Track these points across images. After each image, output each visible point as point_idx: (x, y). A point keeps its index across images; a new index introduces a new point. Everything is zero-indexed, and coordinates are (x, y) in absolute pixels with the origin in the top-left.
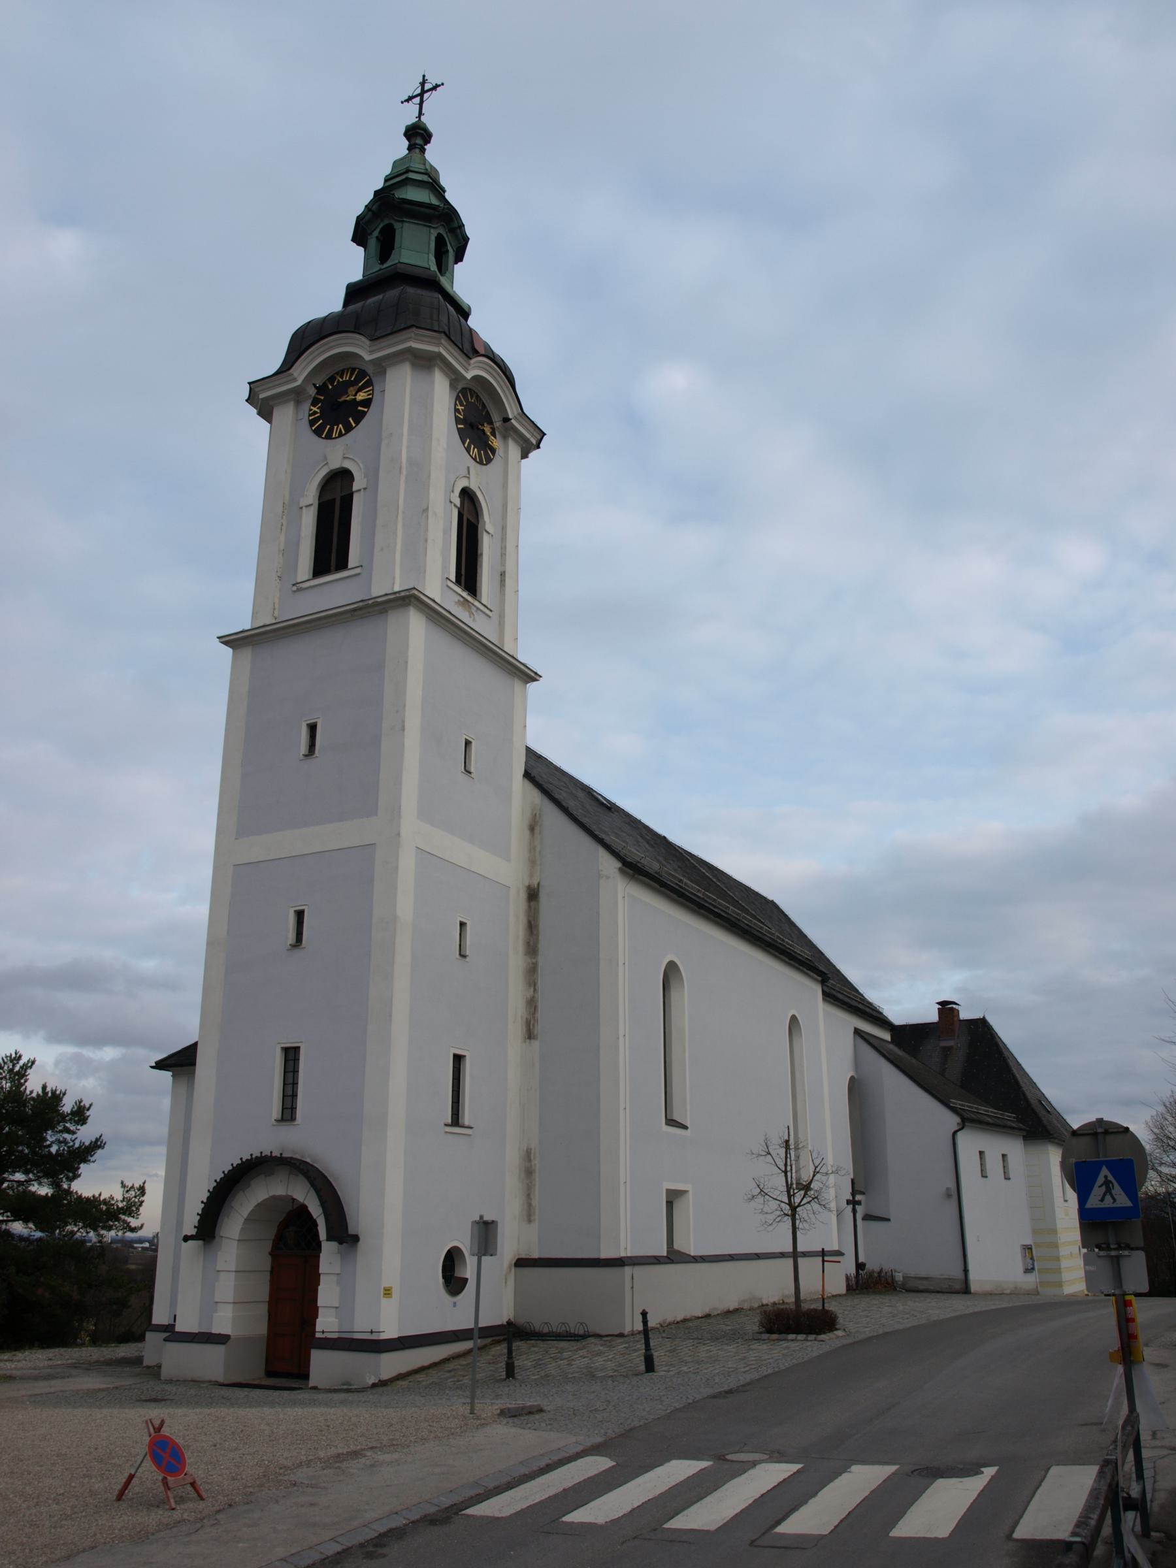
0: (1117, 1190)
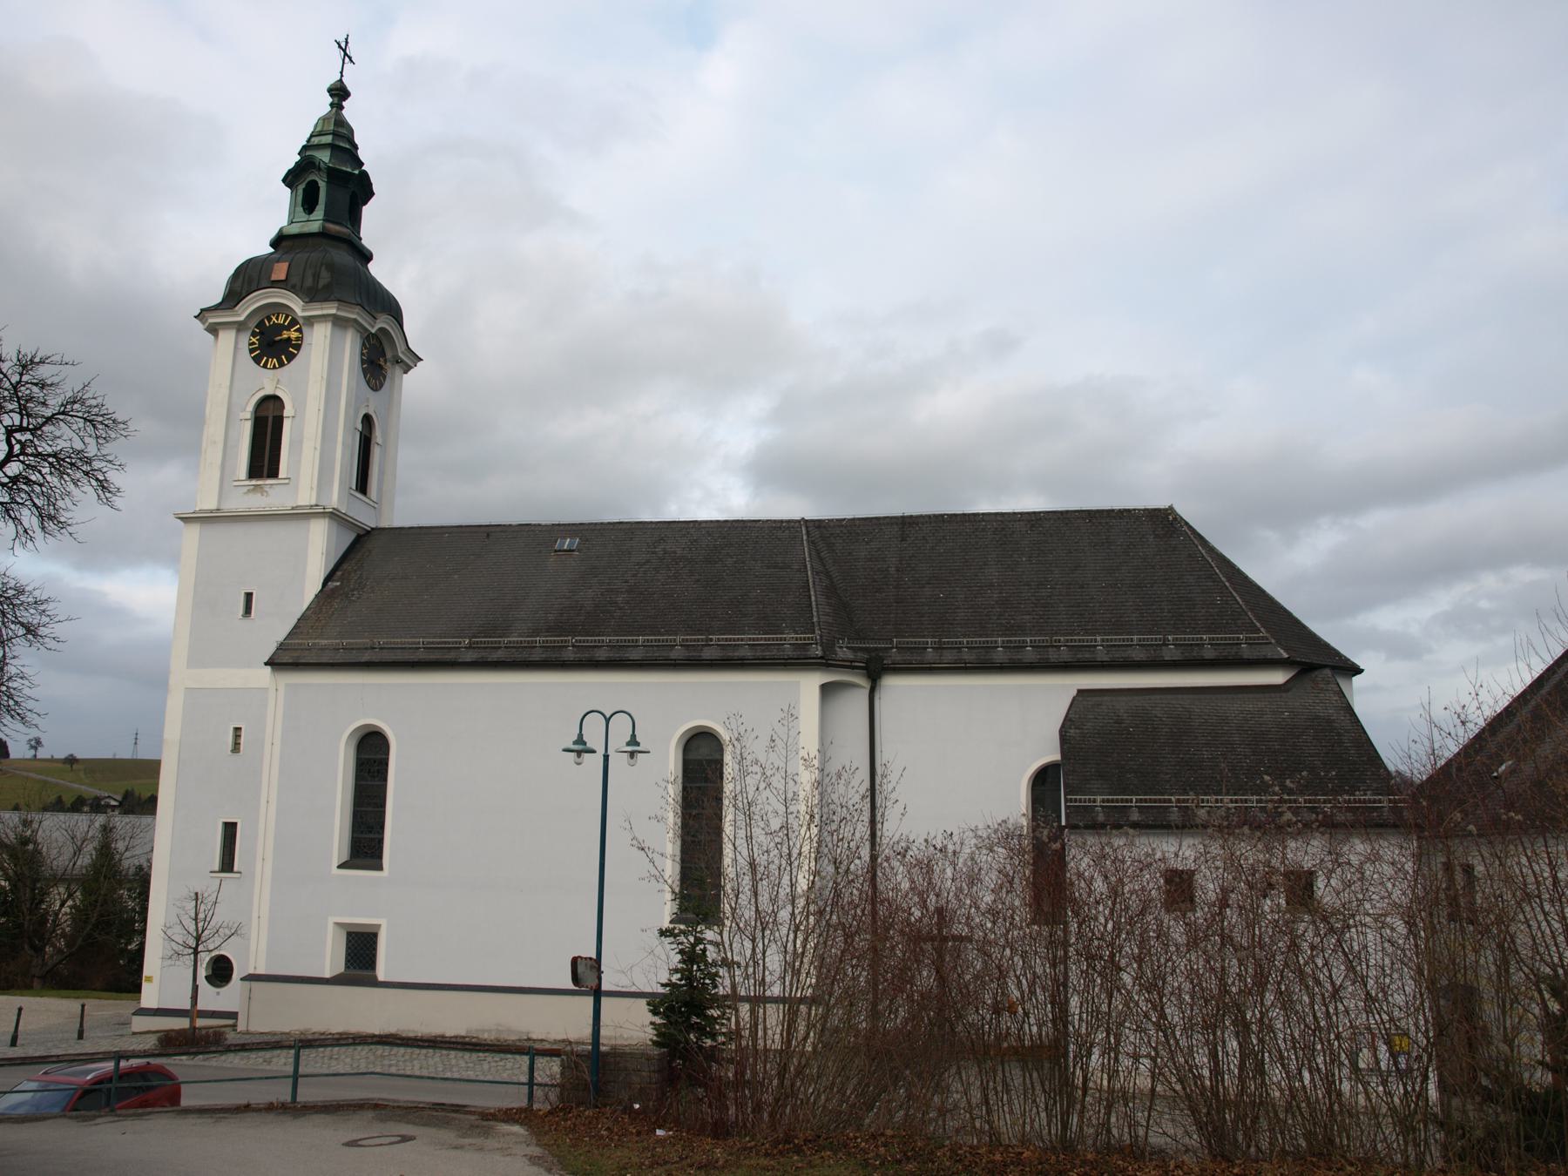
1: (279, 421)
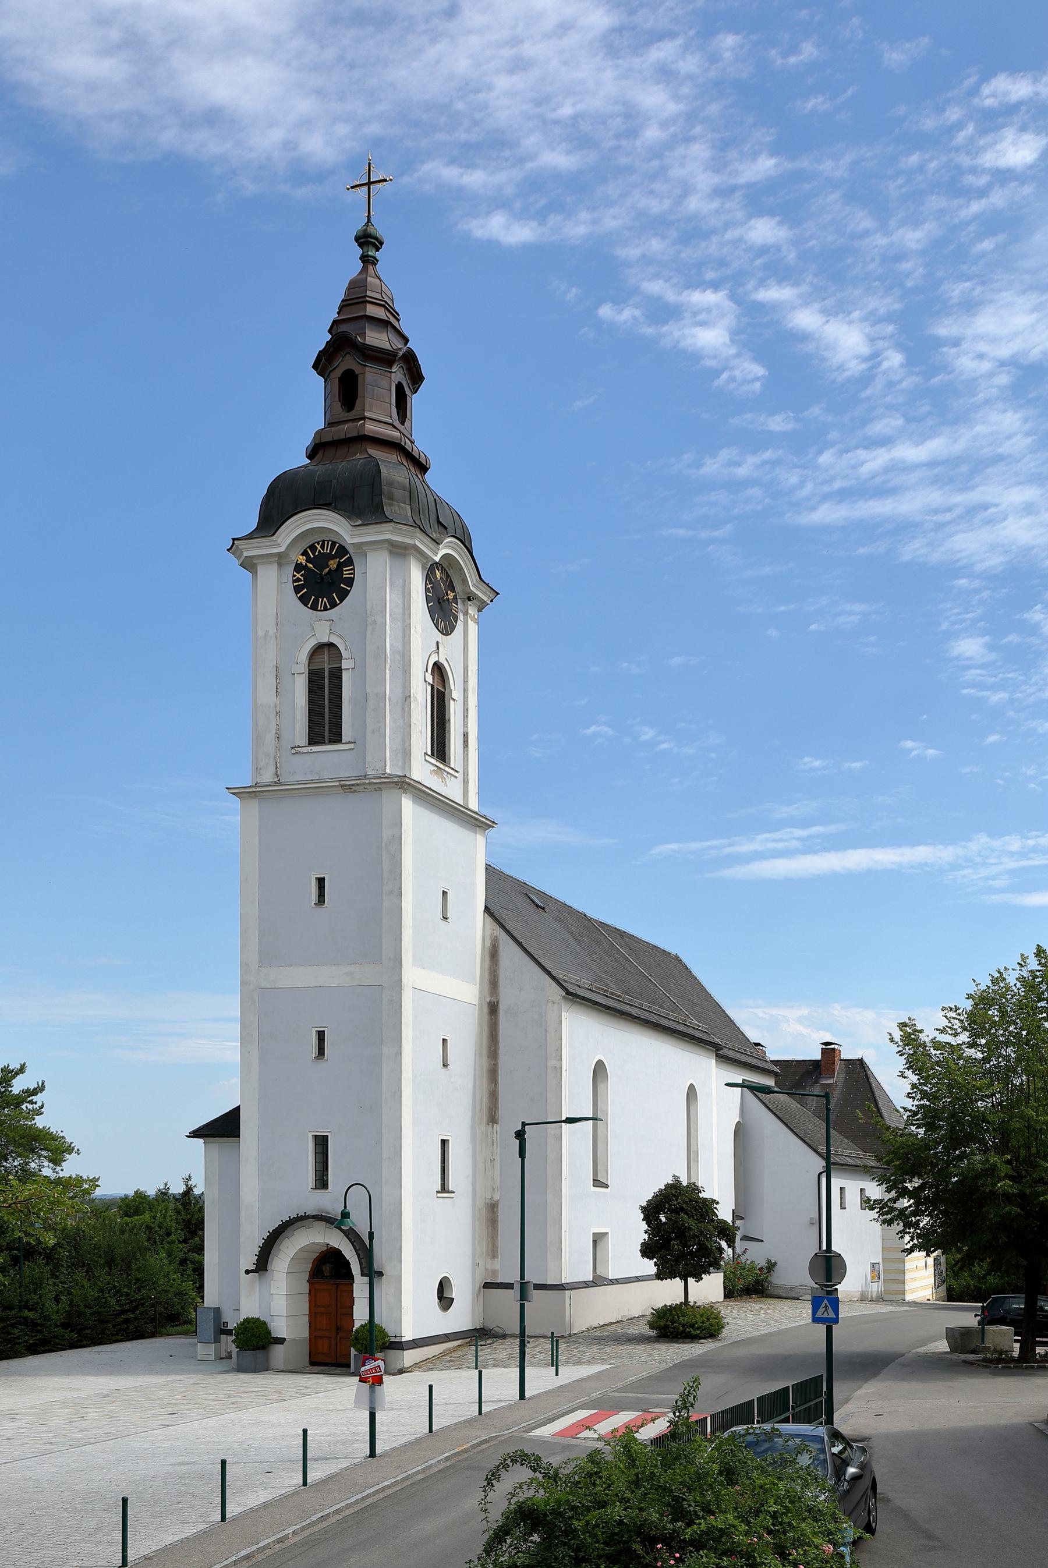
0: (830, 1310)
1: (337, 674)
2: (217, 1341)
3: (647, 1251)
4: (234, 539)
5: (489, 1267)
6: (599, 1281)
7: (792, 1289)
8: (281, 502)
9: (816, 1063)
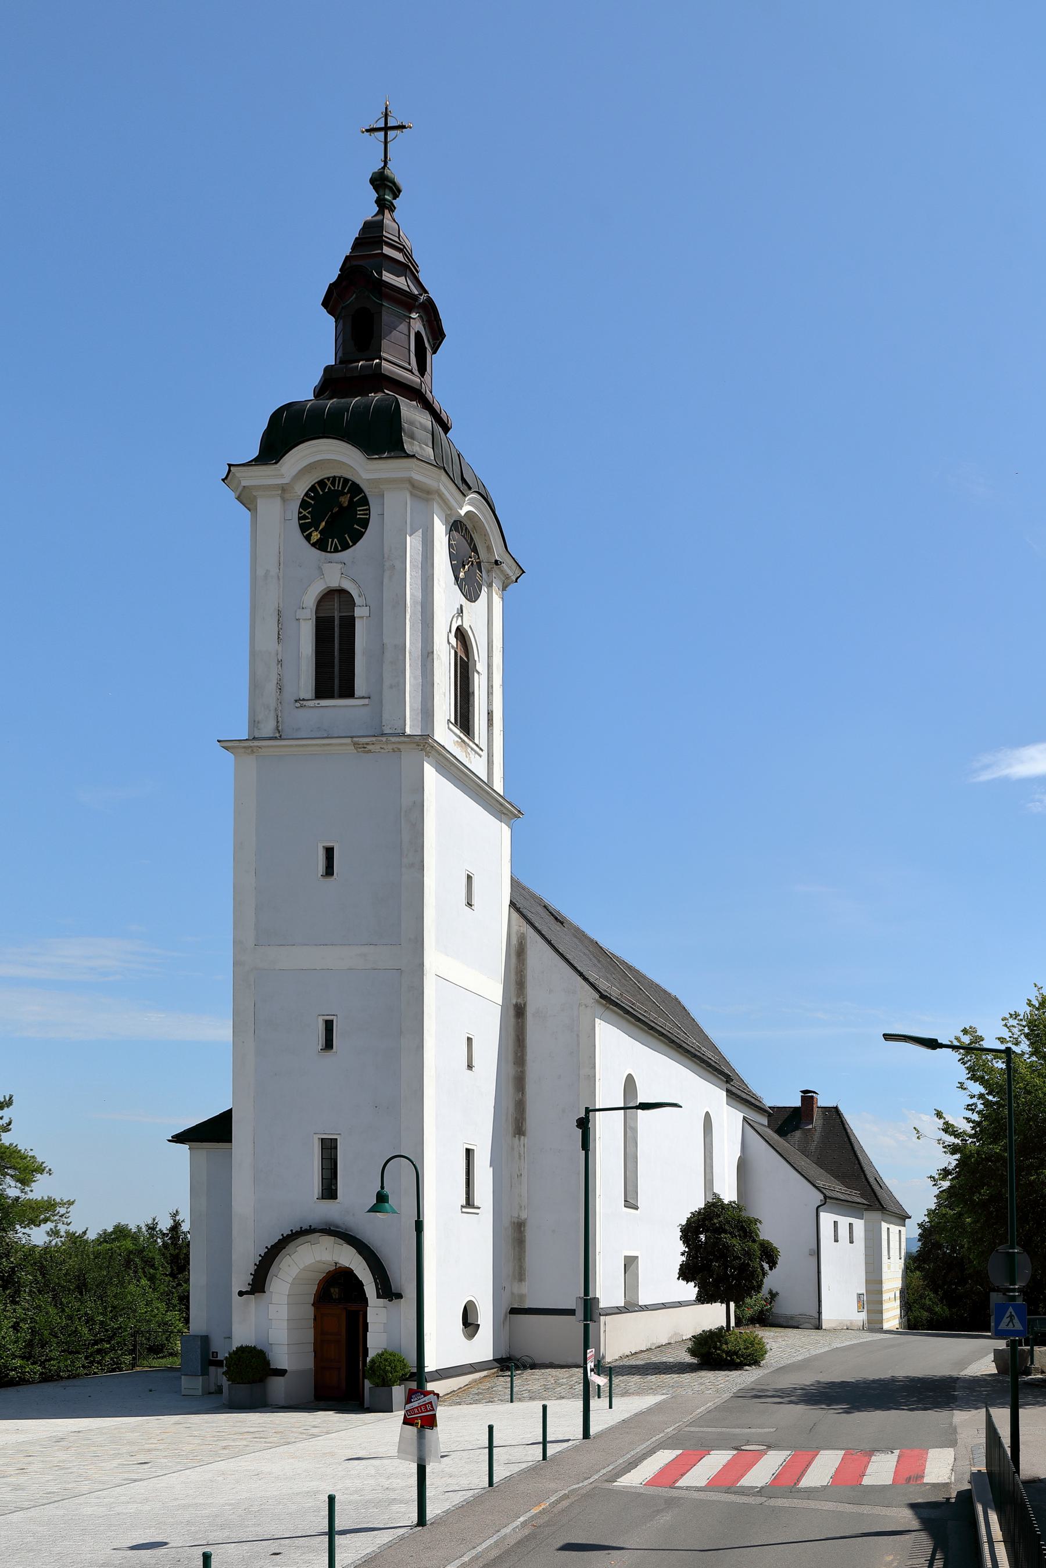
0: (1016, 1320)
1: (349, 624)
2: (205, 1373)
3: (686, 1273)
4: (230, 465)
5: (516, 1291)
6: (630, 1307)
7: (792, 1318)
8: (285, 431)
9: (796, 1109)
